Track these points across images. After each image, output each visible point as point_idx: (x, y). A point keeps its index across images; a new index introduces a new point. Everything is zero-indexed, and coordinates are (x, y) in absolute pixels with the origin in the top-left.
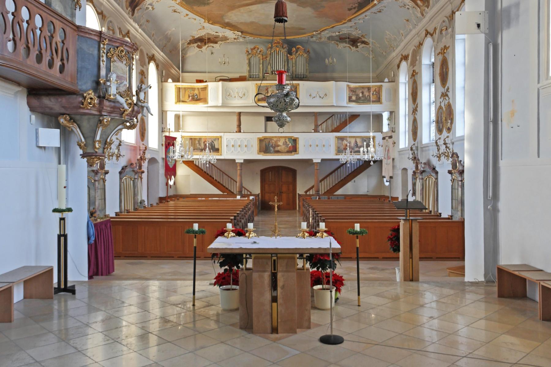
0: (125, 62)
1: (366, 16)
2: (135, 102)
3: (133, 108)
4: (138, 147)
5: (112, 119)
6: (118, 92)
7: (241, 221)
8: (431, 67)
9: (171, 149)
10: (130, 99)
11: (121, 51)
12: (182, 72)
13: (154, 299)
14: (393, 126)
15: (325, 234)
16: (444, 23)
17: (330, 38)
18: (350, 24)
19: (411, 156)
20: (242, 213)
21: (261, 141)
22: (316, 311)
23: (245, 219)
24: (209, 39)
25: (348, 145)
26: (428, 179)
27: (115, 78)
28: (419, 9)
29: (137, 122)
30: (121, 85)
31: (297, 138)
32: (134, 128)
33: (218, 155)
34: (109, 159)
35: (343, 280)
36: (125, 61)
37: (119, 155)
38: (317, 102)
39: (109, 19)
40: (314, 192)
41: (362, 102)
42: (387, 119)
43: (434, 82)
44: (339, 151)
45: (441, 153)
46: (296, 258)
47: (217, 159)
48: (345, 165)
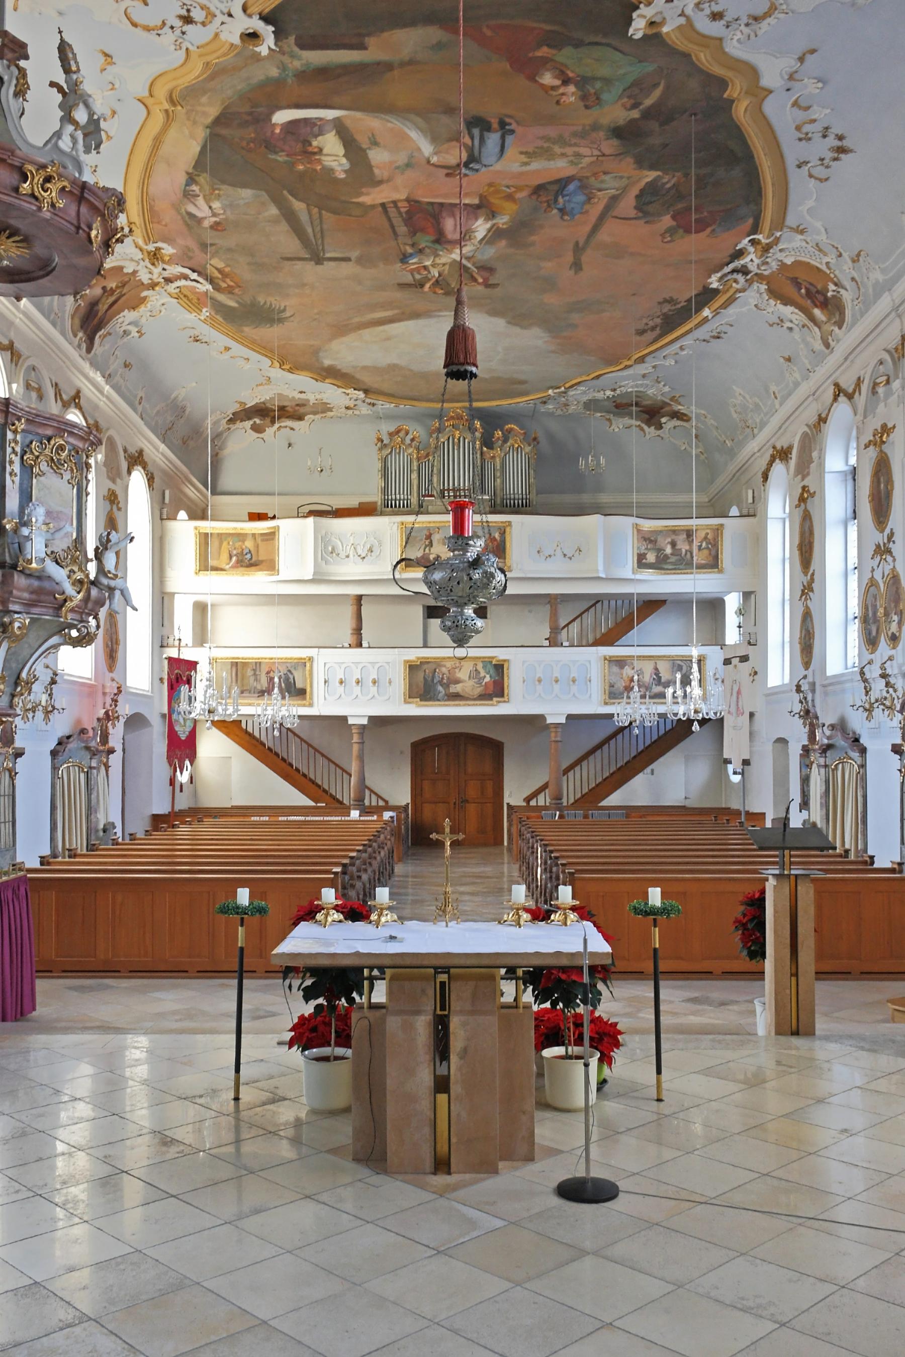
0: (67, 476)
1: (682, 348)
2: (92, 576)
3: (88, 592)
4: (100, 687)
5: (33, 621)
6: (49, 553)
7: (359, 877)
8: (850, 477)
9: (182, 693)
10: (80, 569)
11: (57, 448)
12: (214, 493)
13: (136, 1084)
14: (752, 629)
15: (573, 916)
16: (881, 367)
17: (591, 405)
18: (641, 369)
19: (797, 708)
20: (364, 855)
21: (413, 668)
22: (548, 1114)
23: (369, 871)
24: (282, 409)
25: (636, 678)
26: (840, 766)
27: (41, 519)
28: (816, 329)
29: (98, 627)
30: (58, 535)
31: (505, 661)
32: (89, 643)
33: (304, 706)
34: (25, 718)
35: (620, 1033)
36: (69, 472)
37: (50, 709)
38: (556, 567)
39: (29, 362)
40: (548, 800)
41: (670, 567)
42: (736, 613)
43: (855, 518)
44: (613, 694)
45: (873, 701)
46: (498, 978)
47: (300, 717)
48: (627, 730)
